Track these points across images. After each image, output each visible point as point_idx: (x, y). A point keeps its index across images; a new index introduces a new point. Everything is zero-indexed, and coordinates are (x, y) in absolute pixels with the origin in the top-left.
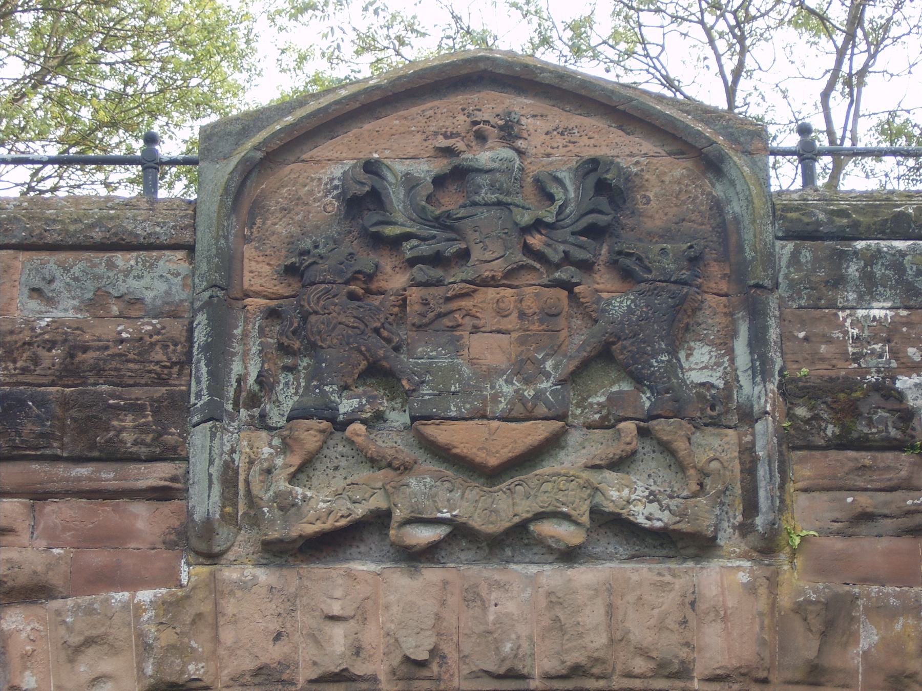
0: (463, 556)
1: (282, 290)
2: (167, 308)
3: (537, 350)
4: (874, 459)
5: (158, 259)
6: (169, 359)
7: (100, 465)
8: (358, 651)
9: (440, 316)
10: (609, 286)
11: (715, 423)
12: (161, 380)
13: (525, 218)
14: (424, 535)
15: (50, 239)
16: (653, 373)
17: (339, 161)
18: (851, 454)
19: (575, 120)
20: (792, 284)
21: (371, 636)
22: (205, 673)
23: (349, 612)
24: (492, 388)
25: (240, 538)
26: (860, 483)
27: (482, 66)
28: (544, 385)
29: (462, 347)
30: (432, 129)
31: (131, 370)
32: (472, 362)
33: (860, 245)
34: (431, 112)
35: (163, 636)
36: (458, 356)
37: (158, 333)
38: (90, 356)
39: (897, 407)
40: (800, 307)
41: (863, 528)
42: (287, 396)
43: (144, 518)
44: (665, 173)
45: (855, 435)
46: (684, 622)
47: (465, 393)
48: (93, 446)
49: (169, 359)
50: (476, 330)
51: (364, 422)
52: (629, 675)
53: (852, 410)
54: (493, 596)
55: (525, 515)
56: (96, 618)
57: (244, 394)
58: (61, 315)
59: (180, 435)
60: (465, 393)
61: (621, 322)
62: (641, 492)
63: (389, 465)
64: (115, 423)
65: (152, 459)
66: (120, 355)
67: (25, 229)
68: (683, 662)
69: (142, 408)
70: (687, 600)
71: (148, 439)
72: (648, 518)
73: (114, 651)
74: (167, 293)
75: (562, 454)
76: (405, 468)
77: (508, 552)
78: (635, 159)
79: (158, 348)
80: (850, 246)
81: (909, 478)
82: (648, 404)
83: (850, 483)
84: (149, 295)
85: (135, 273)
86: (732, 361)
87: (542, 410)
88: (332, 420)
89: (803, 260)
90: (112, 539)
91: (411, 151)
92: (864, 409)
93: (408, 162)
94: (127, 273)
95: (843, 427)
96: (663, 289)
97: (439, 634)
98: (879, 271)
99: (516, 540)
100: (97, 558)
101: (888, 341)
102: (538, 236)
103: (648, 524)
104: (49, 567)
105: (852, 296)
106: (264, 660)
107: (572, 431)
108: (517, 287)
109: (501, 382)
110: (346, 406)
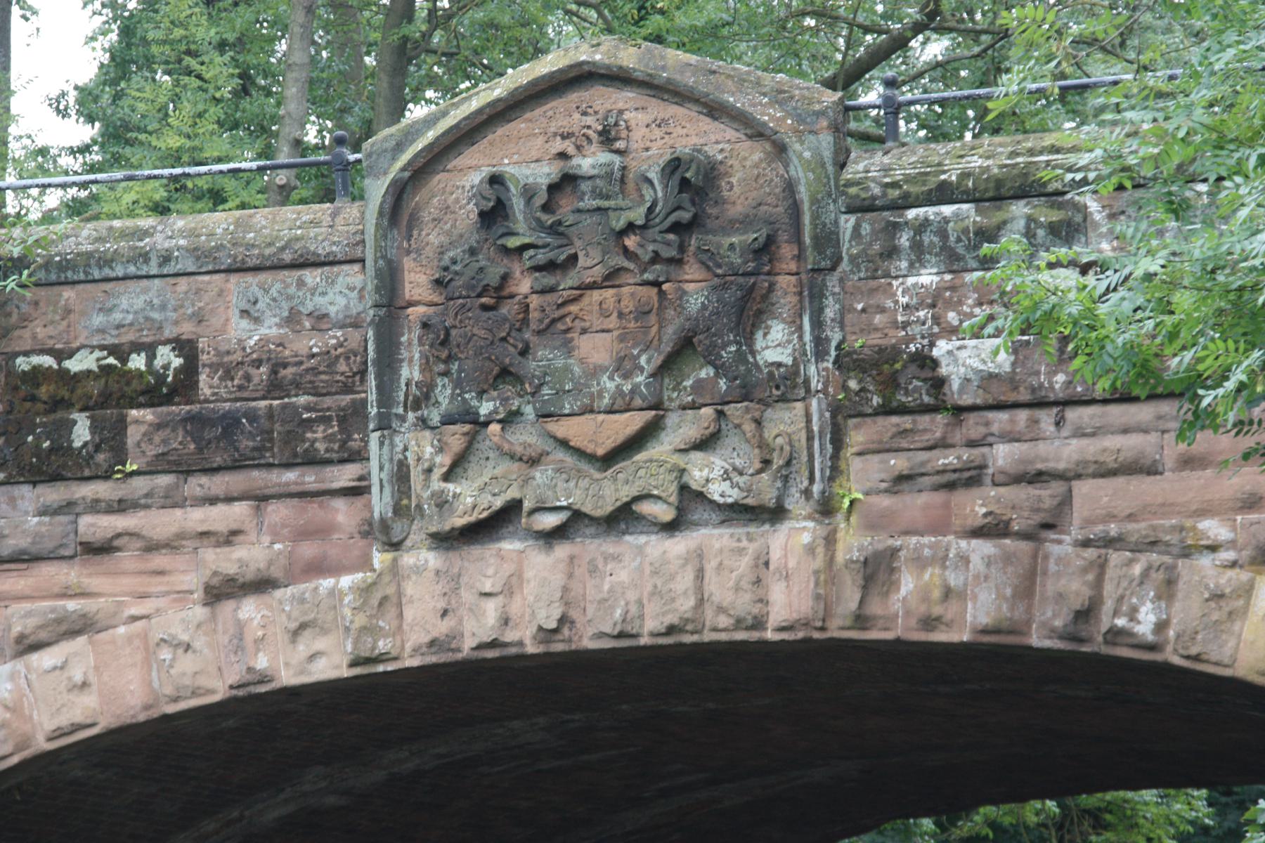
0: (588, 531)
1: (436, 298)
2: (348, 321)
3: (634, 347)
4: (914, 422)
5: (338, 275)
6: (351, 369)
7: (305, 469)
8: (506, 621)
9: (554, 321)
10: (696, 276)
11: (783, 399)
12: (347, 389)
13: (620, 224)
14: (550, 521)
15: (251, 263)
16: (724, 363)
17: (477, 168)
18: (895, 419)
19: (673, 110)
20: (853, 259)
21: (515, 608)
22: (393, 646)
23: (497, 589)
24: (598, 384)
25: (414, 527)
26: (905, 445)
27: (586, 68)
28: (640, 379)
29: (573, 349)
30: (553, 129)
31: (322, 381)
32: (581, 361)
33: (911, 214)
34: (550, 113)
35: (357, 619)
36: (570, 357)
37: (341, 345)
38: (288, 372)
39: (930, 375)
40: (860, 279)
41: (905, 486)
42: (444, 394)
43: (343, 513)
44: (745, 159)
45: (895, 404)
46: (758, 581)
47: (578, 389)
48: (295, 455)
49: (351, 369)
50: (584, 331)
51: (499, 421)
52: (715, 630)
53: (891, 383)
54: (609, 567)
55: (625, 500)
56: (307, 606)
57: (411, 398)
58: (267, 331)
59: (362, 440)
60: (578, 389)
61: (697, 319)
62: (717, 472)
63: (521, 459)
64: (309, 435)
65: (342, 461)
66: (313, 369)
67: (230, 256)
68: (755, 618)
69: (329, 419)
70: (761, 561)
71: (336, 447)
72: (722, 496)
73: (324, 631)
74: (347, 307)
75: (663, 434)
76: (534, 462)
77: (623, 526)
78: (720, 146)
79: (341, 360)
80: (901, 216)
81: (944, 438)
82: (724, 388)
83: (895, 446)
84: (332, 310)
85: (320, 290)
86: (801, 338)
87: (638, 402)
88: (475, 422)
89: (863, 233)
90: (322, 532)
91: (534, 154)
92: (902, 381)
93: (532, 165)
94: (313, 291)
95: (884, 397)
96: (732, 283)
97: (566, 604)
98: (927, 238)
99: (623, 518)
100: (308, 550)
101: (933, 306)
102: (633, 237)
103: (721, 500)
104: (270, 563)
105: (904, 264)
106: (435, 634)
107: (670, 413)
108: (619, 286)
109: (605, 378)
110: (485, 408)
